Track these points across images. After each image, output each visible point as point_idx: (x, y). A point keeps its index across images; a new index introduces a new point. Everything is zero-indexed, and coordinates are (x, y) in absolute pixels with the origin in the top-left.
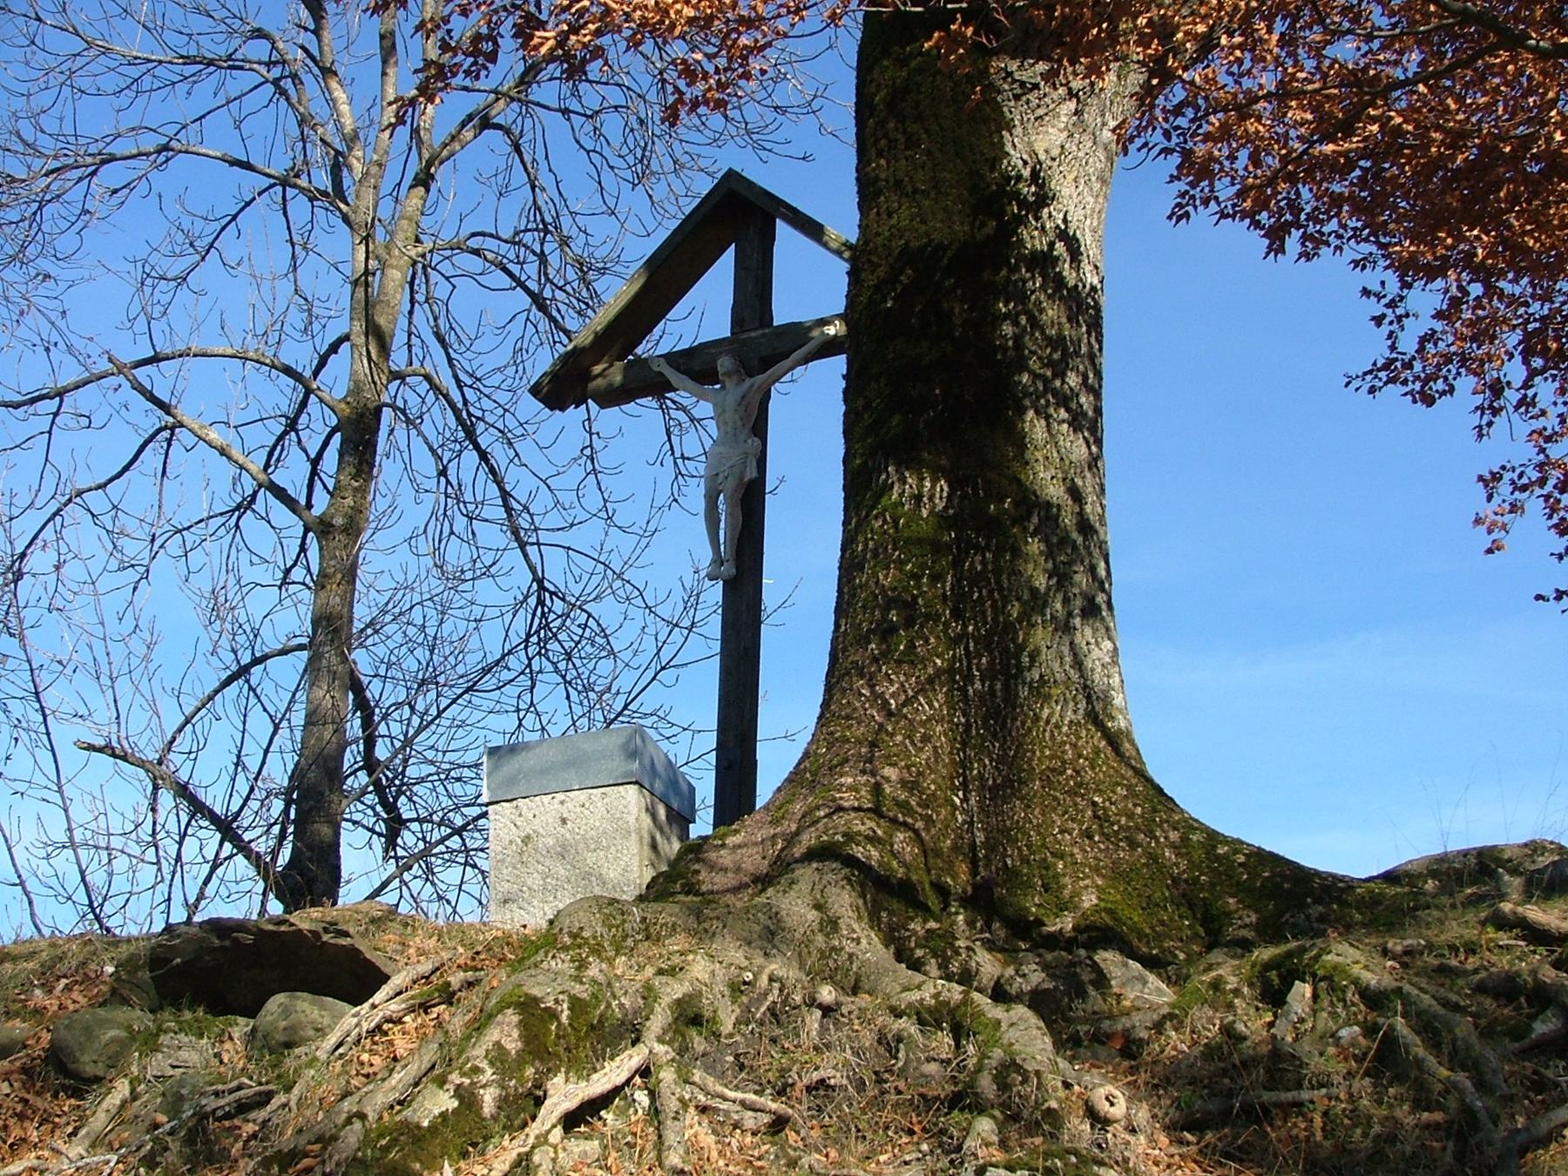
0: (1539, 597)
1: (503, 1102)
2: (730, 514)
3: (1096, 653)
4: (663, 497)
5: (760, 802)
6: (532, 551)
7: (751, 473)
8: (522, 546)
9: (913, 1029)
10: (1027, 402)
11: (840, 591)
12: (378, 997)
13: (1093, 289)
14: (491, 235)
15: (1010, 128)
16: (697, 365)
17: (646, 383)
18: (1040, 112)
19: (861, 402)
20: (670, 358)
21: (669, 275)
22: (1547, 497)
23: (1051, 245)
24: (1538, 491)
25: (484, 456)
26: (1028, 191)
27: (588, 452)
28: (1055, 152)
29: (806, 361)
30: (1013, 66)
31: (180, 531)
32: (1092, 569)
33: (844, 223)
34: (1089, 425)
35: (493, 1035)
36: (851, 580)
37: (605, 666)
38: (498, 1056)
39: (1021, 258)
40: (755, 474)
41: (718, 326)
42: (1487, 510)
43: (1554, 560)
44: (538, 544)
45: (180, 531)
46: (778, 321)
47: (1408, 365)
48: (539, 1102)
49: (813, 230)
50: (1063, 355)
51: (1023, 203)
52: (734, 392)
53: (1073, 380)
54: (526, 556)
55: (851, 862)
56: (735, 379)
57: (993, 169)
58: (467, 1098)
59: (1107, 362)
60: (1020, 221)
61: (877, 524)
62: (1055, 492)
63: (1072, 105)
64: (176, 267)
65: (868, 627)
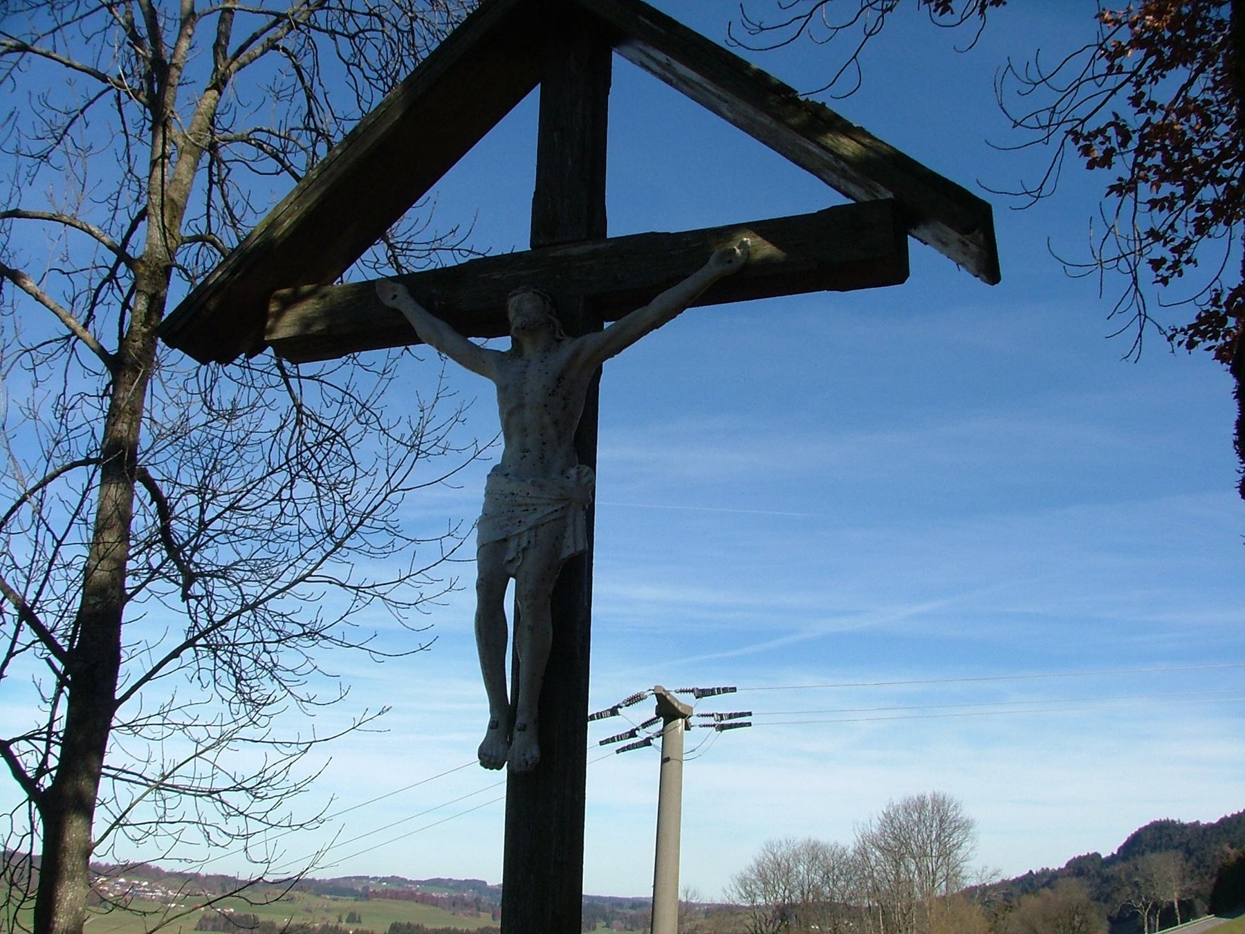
6: (294, 382)
16: (458, 304)
17: (367, 325)
31: (28, 351)
37: (349, 473)
44: (299, 377)
45: (28, 351)
46: (615, 229)
64: (38, 148)
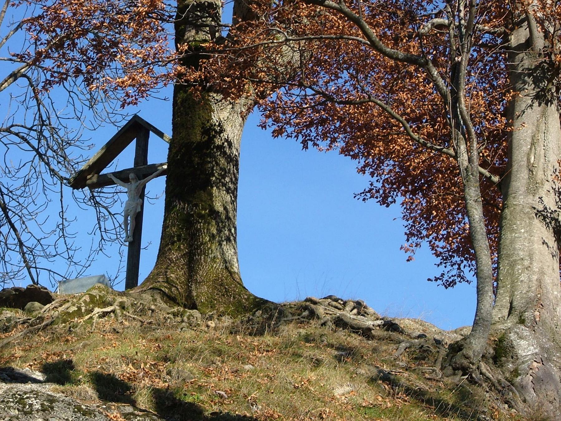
0: (429, 280)
1: (86, 310)
2: (132, 222)
3: (230, 252)
4: (96, 246)
5: (139, 285)
6: (33, 271)
7: (139, 210)
8: (29, 268)
9: (172, 317)
10: (214, 185)
11: (162, 233)
12: (53, 303)
13: (236, 155)
14: (22, 126)
15: (213, 111)
16: (123, 176)
18: (222, 108)
19: (170, 184)
20: (114, 174)
21: (113, 149)
22: (430, 242)
23: (223, 143)
24: (426, 239)
25: (12, 226)
26: (218, 129)
27: (61, 227)
28: (226, 119)
29: (157, 176)
30: (215, 95)
32: (230, 230)
33: (169, 134)
34: (233, 192)
35: (84, 298)
36: (165, 230)
38: (85, 302)
39: (214, 147)
40: (140, 210)
41: (131, 165)
42: (406, 245)
43: (436, 266)
44: (36, 268)
46: (149, 163)
47: (378, 191)
48: (92, 312)
49: (160, 134)
50: (224, 173)
51: (216, 132)
52: (134, 185)
53: (227, 179)
54: (30, 273)
55: (161, 290)
56: (135, 180)
57: (208, 122)
58: (79, 308)
59: (240, 177)
60: (215, 137)
61: (173, 215)
62: (221, 209)
63: (231, 106)
65: (167, 241)
